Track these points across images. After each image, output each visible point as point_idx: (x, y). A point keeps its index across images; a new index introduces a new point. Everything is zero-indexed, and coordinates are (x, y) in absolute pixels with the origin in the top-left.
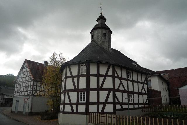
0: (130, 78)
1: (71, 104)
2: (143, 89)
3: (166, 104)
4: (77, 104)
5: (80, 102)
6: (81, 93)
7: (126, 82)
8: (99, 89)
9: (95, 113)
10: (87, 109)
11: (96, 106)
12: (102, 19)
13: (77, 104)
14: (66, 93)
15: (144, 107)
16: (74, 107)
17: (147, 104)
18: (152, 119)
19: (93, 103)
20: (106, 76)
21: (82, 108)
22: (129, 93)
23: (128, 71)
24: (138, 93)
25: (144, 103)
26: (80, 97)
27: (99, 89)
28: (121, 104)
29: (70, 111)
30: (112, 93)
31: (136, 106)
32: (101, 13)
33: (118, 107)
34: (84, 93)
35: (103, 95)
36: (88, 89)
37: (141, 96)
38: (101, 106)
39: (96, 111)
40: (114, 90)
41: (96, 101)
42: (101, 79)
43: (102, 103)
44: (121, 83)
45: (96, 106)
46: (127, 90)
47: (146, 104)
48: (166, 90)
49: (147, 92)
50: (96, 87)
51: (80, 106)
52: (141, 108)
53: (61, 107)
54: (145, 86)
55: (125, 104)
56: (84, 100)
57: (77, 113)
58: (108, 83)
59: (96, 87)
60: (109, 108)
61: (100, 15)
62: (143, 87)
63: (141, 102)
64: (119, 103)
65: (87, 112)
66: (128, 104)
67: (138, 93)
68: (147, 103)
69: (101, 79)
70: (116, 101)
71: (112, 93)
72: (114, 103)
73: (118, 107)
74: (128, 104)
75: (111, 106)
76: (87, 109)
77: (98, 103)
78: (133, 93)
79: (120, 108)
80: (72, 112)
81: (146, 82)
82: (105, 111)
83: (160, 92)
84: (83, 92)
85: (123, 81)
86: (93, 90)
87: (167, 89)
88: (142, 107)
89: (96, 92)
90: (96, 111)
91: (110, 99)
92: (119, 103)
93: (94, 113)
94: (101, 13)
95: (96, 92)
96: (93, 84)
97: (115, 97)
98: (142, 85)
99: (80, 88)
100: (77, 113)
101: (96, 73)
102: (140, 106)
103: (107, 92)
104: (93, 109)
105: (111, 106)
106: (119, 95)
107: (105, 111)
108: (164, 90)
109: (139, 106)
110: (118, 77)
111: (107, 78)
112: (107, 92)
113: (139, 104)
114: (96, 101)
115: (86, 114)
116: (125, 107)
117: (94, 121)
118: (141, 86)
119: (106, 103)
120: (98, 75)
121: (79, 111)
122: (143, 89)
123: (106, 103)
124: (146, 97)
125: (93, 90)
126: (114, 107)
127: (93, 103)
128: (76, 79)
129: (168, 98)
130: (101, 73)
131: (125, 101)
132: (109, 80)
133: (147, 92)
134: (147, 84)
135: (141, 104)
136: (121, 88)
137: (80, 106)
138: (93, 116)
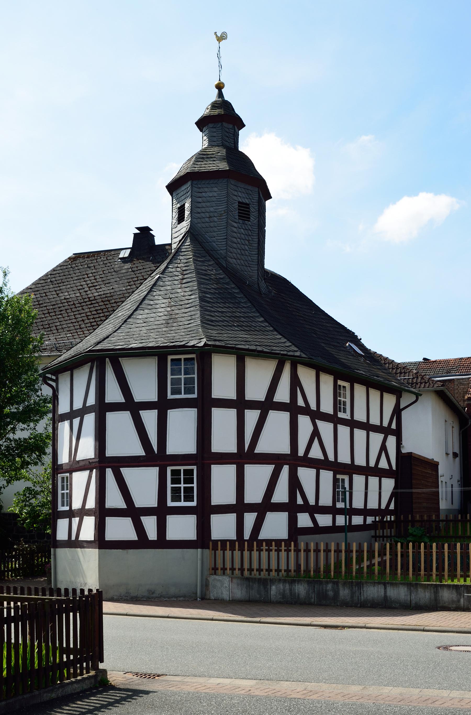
0: (345, 412)
1: (133, 512)
2: (316, 441)
3: (449, 511)
4: (161, 512)
5: (170, 504)
6: (175, 473)
7: (330, 426)
8: (244, 457)
9: (232, 542)
10: (204, 528)
11: (232, 518)
12: (222, 122)
13: (161, 512)
14: (109, 473)
15: (381, 521)
16: (150, 524)
17: (390, 513)
18: (59, 644)
19: (223, 509)
20: (267, 405)
21: (182, 527)
22: (337, 468)
23: (340, 382)
24: (367, 471)
25: (383, 506)
26: (169, 486)
27: (244, 457)
28: (314, 510)
29: (132, 536)
30: (286, 470)
31: (357, 520)
32: (220, 87)
33: (304, 520)
34: (189, 473)
35: (257, 478)
36: (205, 457)
37: (373, 481)
38: (250, 519)
39: (233, 536)
40: (294, 460)
41: (231, 499)
42: (252, 417)
43: (252, 508)
44: (316, 434)
45: (232, 518)
46: (331, 457)
47: (387, 511)
48: (455, 455)
49: (394, 468)
50: (233, 449)
51: (171, 520)
52: (374, 525)
53: (62, 524)
54: (391, 441)
55: (324, 510)
56: (189, 498)
57: (162, 542)
58: (275, 436)
59: (233, 449)
60: (276, 526)
61: (213, 96)
62: (383, 448)
63: (373, 504)
64: (306, 508)
65: (204, 538)
66: (332, 510)
67: (367, 471)
68: (392, 507)
69: (252, 417)
70: (300, 501)
71: (286, 470)
72: (291, 508)
73: (304, 520)
74: (332, 510)
75: (283, 517)
76: (204, 528)
77: (239, 508)
78: (351, 469)
79: (310, 524)
80: (142, 542)
81: (394, 426)
82: (264, 535)
83: (434, 466)
84: (182, 468)
85: (321, 424)
86: (224, 458)
87: (457, 450)
88: (374, 522)
89: (231, 469)
90: (233, 536)
91: (281, 495)
92: (306, 508)
93: (224, 542)
94: (220, 87)
95: (231, 469)
96: (224, 439)
97: (295, 485)
98: (381, 437)
99: (171, 449)
100: (162, 542)
101: (232, 394)
102: (370, 520)
103: (269, 469)
104: (223, 527)
105: (283, 517)
106: (306, 475)
107: (264, 535)
108: (447, 454)
109: (365, 520)
110: (306, 410)
111: (273, 415)
112: (269, 469)
113: (365, 512)
114: (231, 499)
115: (202, 548)
116: (324, 520)
117: (233, 569)
118: (376, 439)
119: (266, 506)
120: (240, 404)
121: (171, 535)
122: (316, 441)
123: (266, 506)
124: (389, 484)
125: (224, 458)
126: (293, 521)
127: (223, 509)
128: (150, 418)
129: (457, 489)
130: (250, 395)
131: (326, 499)
132: (278, 421)
133: (394, 468)
134: (398, 433)
135: (372, 512)
136: (316, 453)
137: (171, 520)
138: (246, 553)
